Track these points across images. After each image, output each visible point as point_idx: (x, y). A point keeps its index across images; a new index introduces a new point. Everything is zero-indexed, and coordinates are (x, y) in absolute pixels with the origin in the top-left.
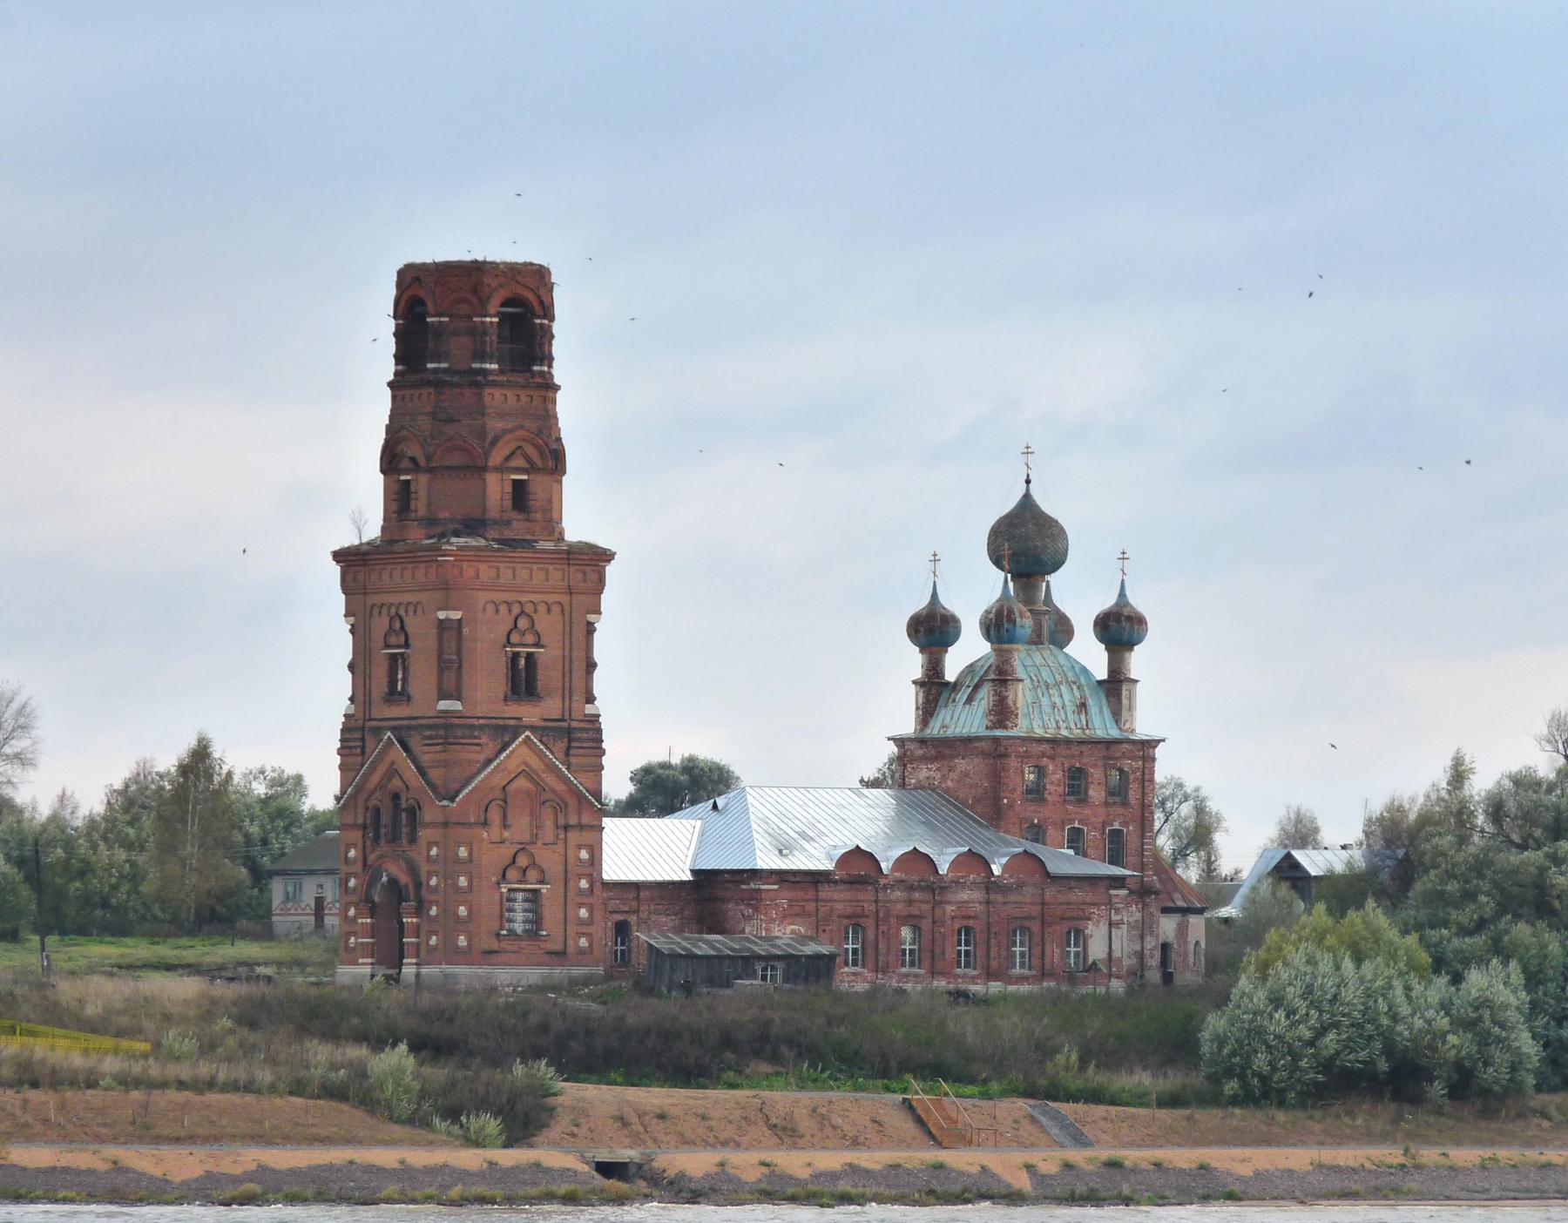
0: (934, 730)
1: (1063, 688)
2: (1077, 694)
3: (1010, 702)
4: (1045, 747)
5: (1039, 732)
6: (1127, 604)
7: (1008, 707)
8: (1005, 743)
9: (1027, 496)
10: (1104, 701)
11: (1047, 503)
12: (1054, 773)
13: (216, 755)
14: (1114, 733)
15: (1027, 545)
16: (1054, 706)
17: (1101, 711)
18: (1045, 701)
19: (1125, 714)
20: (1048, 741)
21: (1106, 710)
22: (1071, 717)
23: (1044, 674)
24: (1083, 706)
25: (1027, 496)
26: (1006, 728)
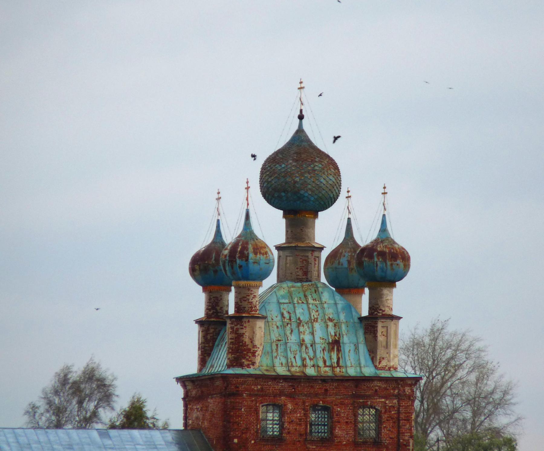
0: (206, 371)
1: (317, 325)
2: (332, 331)
3: (246, 339)
4: (282, 385)
5: (281, 371)
6: (252, 233)
7: (245, 345)
8: (234, 381)
9: (300, 131)
10: (361, 339)
11: (321, 140)
12: (294, 411)
13: (149, 414)
14: (369, 371)
15: (299, 179)
16: (302, 343)
17: (357, 348)
18: (293, 338)
19: (381, 352)
20: (285, 378)
21: (363, 348)
22: (319, 354)
23: (299, 311)
24: (335, 344)
25: (300, 131)
26: (241, 366)
